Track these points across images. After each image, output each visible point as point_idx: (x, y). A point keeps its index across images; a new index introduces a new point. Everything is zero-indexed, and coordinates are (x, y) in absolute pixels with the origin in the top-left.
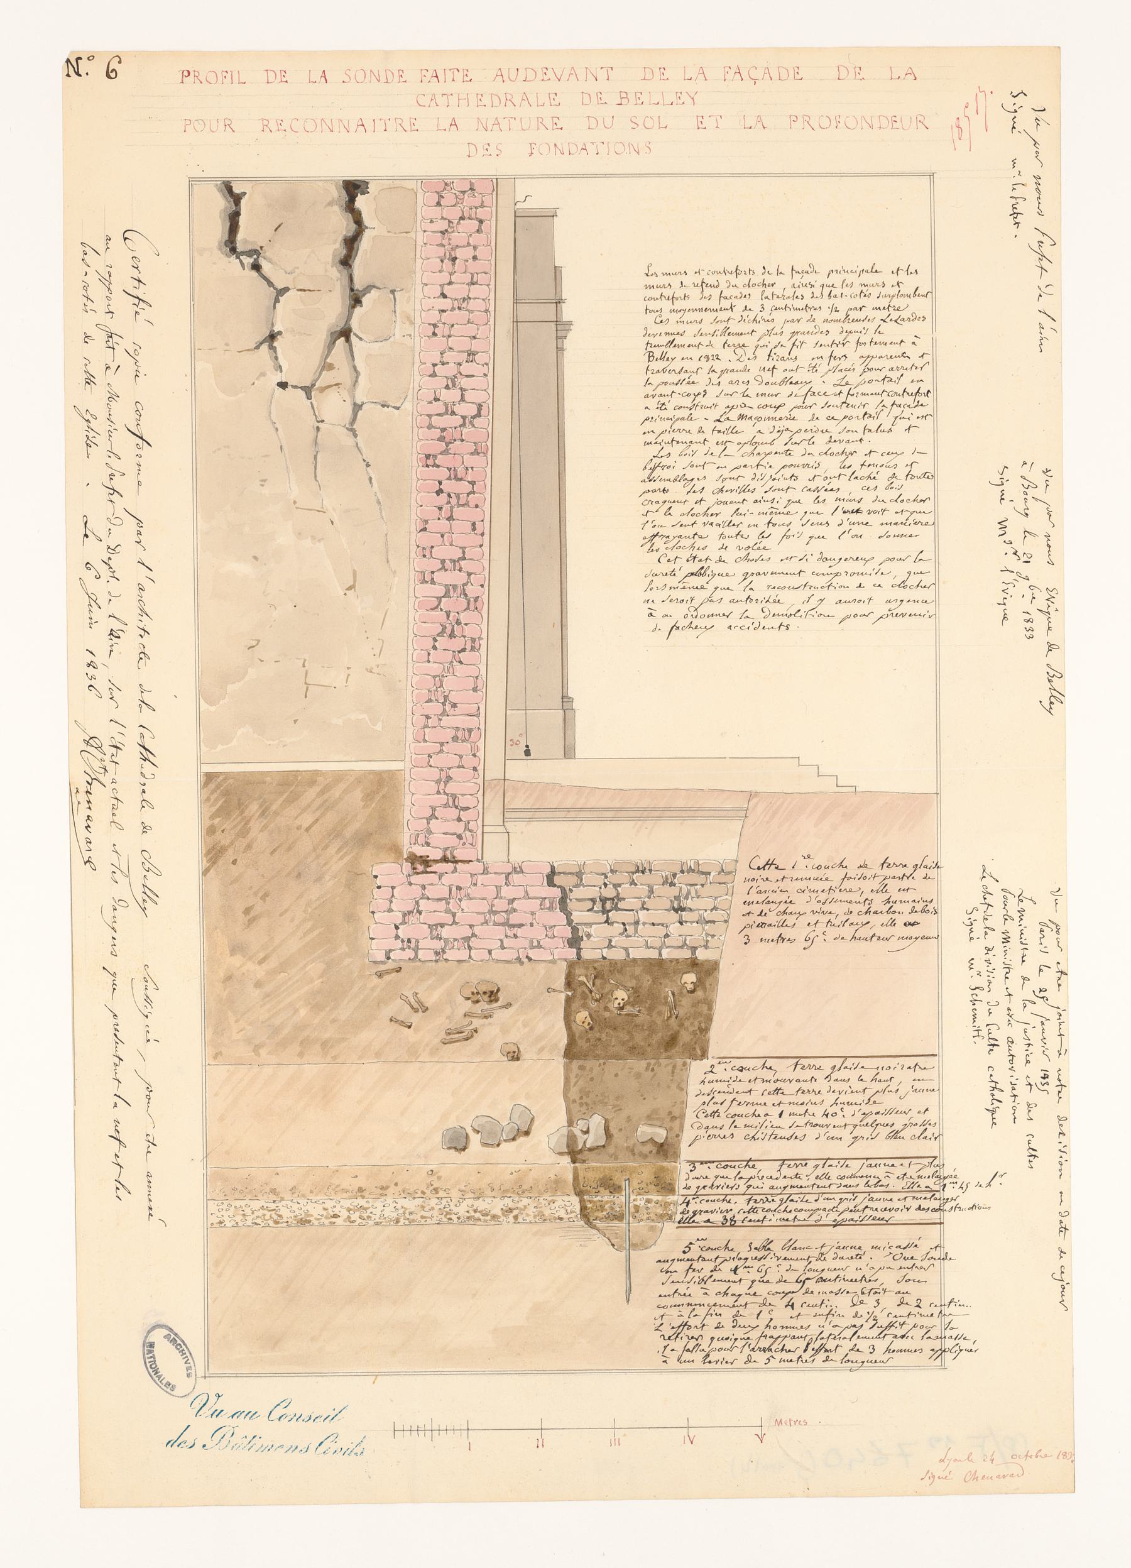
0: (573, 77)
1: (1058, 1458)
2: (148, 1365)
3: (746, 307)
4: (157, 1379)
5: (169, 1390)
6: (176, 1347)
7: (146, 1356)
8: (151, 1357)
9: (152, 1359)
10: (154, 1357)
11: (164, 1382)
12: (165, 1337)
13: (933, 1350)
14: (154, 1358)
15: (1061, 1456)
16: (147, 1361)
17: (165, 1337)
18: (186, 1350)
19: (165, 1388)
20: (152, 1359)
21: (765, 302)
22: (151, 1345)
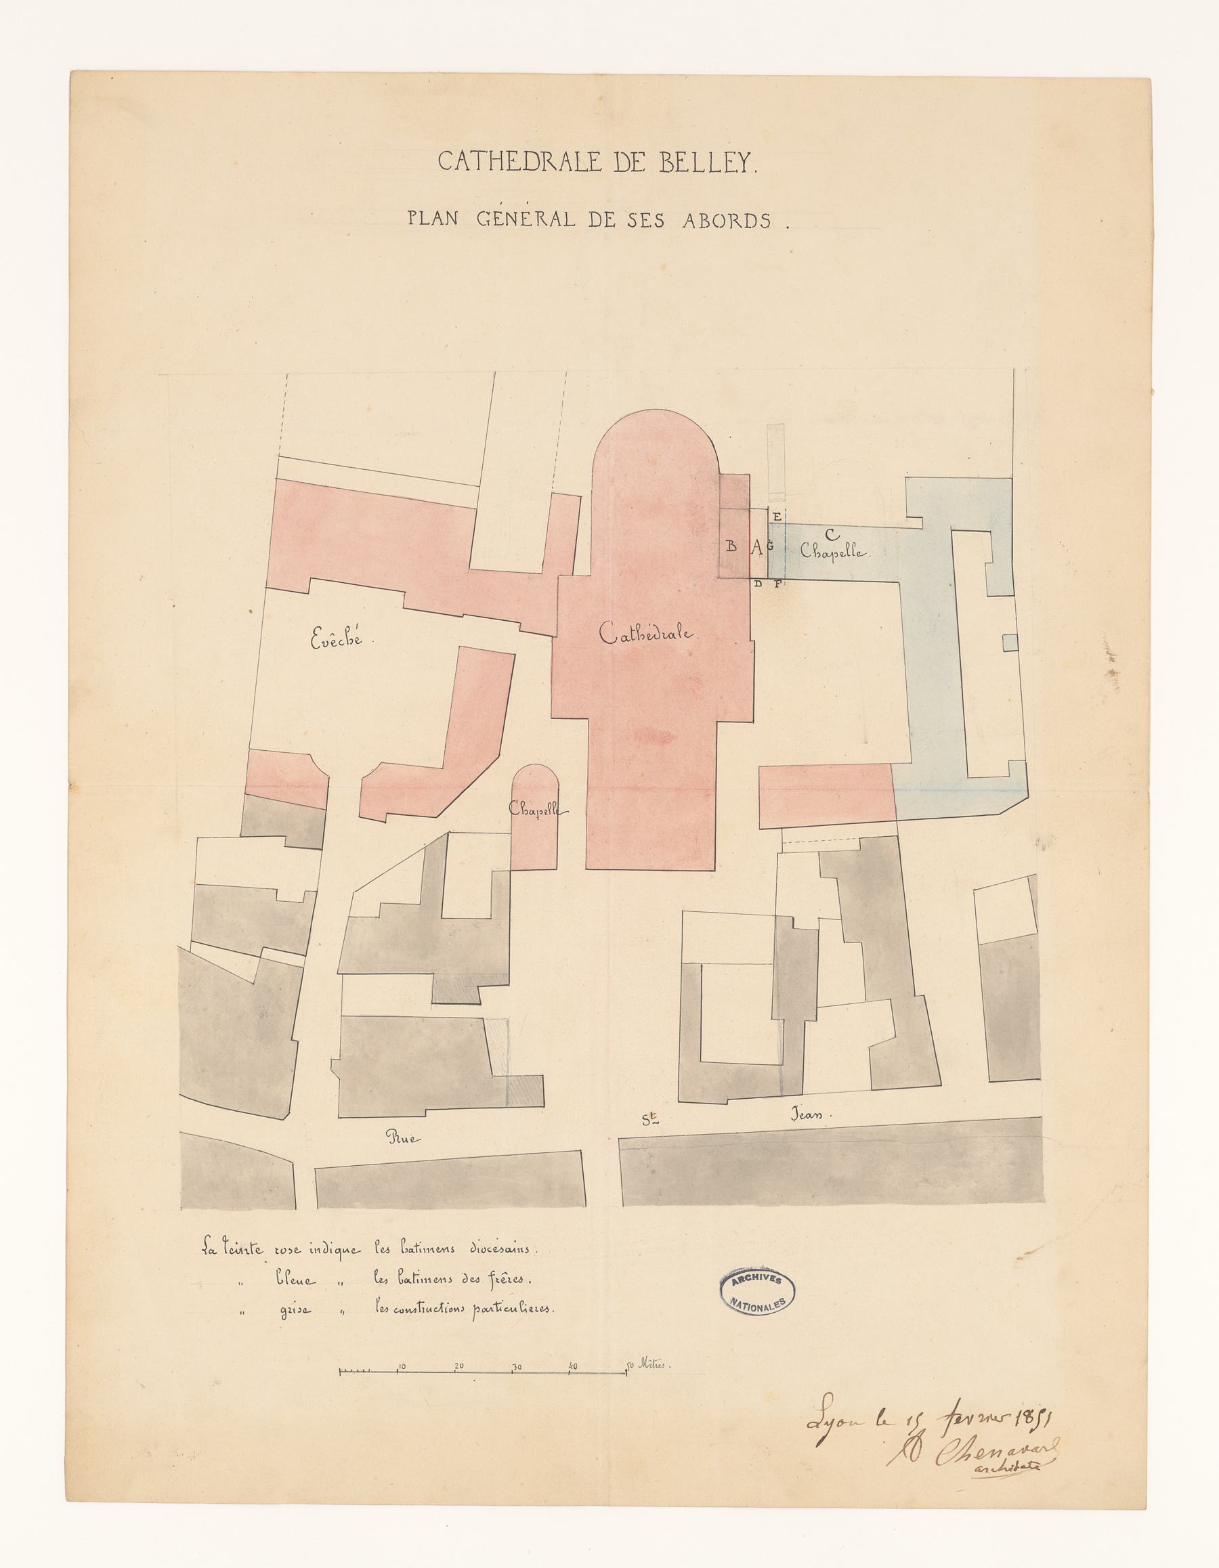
0: (556, 222)
1: (973, 1416)
2: (750, 1312)
3: (203, 1250)
4: (767, 1312)
5: (782, 1306)
6: (748, 1280)
7: (742, 1310)
8: (745, 1307)
9: (747, 1306)
10: (746, 1304)
11: (773, 1306)
12: (734, 1285)
13: (513, 160)
14: (747, 1304)
15: (1023, 1418)
16: (746, 1311)
17: (734, 1285)
18: (755, 1273)
19: (779, 1308)
20: (747, 1306)
21: (492, 214)
22: (734, 1301)
